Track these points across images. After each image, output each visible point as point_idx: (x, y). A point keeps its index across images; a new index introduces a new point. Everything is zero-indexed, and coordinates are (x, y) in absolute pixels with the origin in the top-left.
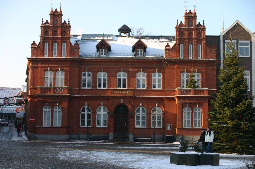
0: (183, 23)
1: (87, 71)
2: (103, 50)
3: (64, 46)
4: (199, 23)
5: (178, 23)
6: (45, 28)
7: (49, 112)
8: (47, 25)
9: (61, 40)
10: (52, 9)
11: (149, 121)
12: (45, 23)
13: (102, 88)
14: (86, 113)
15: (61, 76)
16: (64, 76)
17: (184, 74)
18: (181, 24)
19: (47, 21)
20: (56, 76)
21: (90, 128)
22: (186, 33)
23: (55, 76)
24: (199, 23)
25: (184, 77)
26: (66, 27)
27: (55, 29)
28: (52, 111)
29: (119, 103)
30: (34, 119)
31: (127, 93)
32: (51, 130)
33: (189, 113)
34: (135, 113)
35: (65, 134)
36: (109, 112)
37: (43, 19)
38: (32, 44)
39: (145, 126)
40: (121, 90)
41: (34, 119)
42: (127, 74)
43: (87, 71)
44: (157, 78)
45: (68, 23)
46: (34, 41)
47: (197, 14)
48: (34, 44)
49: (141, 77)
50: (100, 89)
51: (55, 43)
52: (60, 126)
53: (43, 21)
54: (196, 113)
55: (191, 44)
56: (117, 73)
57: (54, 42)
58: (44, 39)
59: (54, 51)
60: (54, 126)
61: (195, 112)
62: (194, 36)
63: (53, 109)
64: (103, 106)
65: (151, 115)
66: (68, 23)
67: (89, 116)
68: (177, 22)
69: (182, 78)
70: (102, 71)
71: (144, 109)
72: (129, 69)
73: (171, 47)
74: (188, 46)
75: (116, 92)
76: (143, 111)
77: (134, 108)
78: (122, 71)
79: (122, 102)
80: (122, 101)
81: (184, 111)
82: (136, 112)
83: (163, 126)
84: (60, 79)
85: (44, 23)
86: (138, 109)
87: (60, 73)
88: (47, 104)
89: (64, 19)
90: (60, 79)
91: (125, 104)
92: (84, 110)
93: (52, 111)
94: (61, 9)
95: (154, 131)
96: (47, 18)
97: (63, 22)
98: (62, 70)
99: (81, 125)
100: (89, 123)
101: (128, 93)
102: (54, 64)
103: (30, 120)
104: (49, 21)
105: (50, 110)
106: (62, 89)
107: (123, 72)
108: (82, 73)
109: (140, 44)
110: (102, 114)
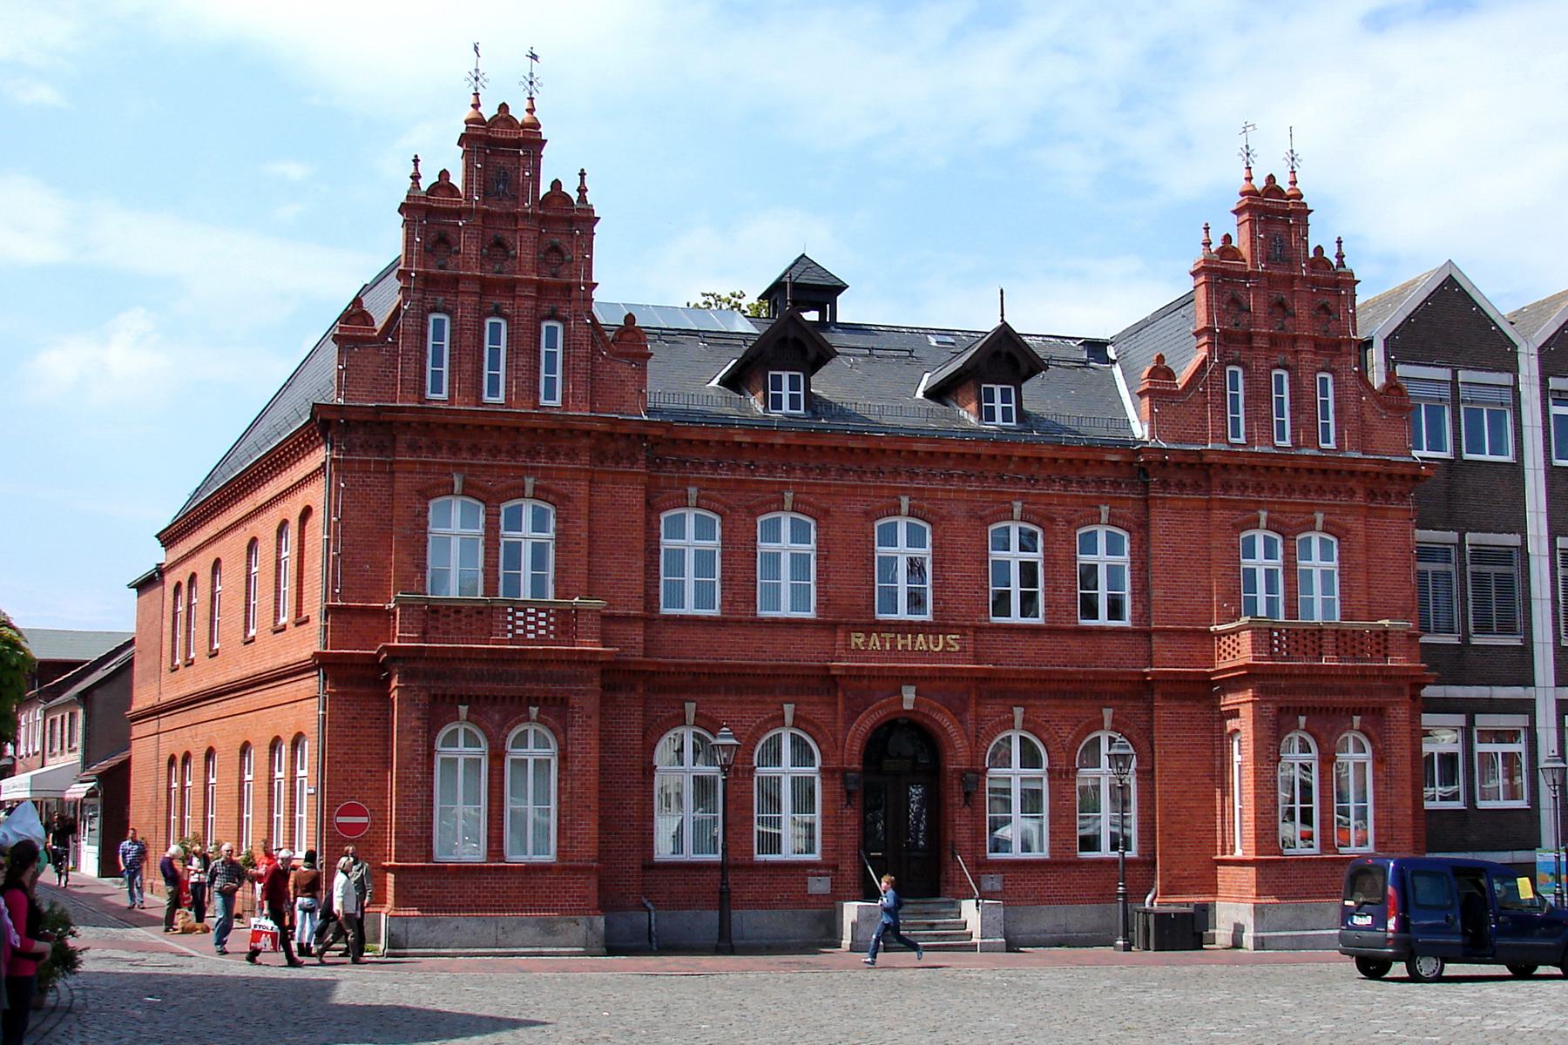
0: (1240, 241)
2: (785, 377)
3: (554, 339)
4: (556, 184)
5: (1207, 244)
6: (426, 211)
7: (473, 764)
8: (441, 201)
9: (537, 299)
10: (476, 106)
12: (433, 189)
13: (1015, 618)
15: (531, 530)
18: (1227, 250)
19: (444, 174)
22: (468, 246)
24: (556, 184)
26: (570, 221)
27: (496, 222)
28: (497, 756)
29: (897, 708)
30: (364, 820)
33: (473, 764)
36: (833, 764)
37: (416, 161)
38: (346, 317)
39: (716, 852)
40: (1102, 631)
41: (364, 820)
45: (575, 196)
46: (1160, 358)
47: (545, 132)
48: (355, 314)
49: (690, 540)
50: (999, 627)
52: (550, 857)
53: (416, 177)
55: (445, 311)
57: (547, 312)
58: (1228, 340)
60: (514, 857)
62: (1303, 319)
64: (794, 726)
66: (575, 196)
68: (412, 170)
71: (1033, 746)
73: (1182, 379)
74: (424, 325)
76: (1030, 759)
77: (977, 742)
79: (908, 706)
80: (909, 694)
81: (442, 752)
83: (823, 852)
84: (455, 544)
85: (424, 185)
89: (557, 167)
90: (455, 544)
91: (925, 715)
93: (497, 756)
94: (531, 111)
95: (724, 877)
97: (545, 188)
98: (540, 493)
101: (946, 644)
102: (496, 452)
103: (364, 814)
104: (457, 180)
105: (481, 751)
106: (543, 615)
108: (663, 517)
109: (1004, 350)
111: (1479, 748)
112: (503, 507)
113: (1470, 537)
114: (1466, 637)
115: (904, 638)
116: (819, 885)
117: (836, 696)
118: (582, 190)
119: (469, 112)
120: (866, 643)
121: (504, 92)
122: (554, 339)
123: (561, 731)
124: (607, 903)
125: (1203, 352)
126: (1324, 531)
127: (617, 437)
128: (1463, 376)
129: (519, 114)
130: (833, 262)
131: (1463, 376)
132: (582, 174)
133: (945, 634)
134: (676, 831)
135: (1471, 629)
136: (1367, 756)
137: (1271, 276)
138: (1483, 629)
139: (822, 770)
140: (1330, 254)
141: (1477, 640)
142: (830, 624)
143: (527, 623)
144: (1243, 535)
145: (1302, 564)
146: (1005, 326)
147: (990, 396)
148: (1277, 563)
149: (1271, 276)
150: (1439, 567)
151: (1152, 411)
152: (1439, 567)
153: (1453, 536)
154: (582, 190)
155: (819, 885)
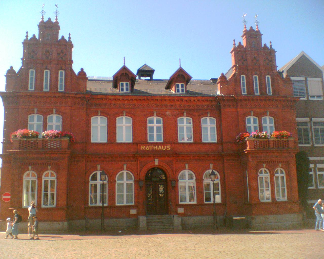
1: (99, 114)
2: (125, 83)
4: (63, 37)
5: (235, 44)
11: (200, 192)
14: (98, 182)
16: (130, 125)
17: (34, 116)
20: (48, 123)
21: (106, 207)
23: (46, 122)
24: (63, 37)
25: (249, 122)
26: (67, 46)
31: (164, 148)
32: (274, 207)
34: (115, 181)
35: (62, 221)
42: (62, 118)
43: (99, 114)
44: (155, 125)
51: (47, 70)
53: (27, 36)
54: (277, 178)
56: (148, 119)
59: (243, 86)
61: (276, 175)
63: (42, 176)
64: (127, 170)
65: (203, 182)
67: (103, 186)
69: (248, 125)
70: (124, 114)
72: (166, 112)
75: (160, 146)
78: (155, 114)
82: (116, 179)
86: (120, 174)
87: (55, 116)
88: (30, 168)
89: (63, 33)
92: (94, 178)
94: (57, 19)
96: (34, 32)
97: (60, 37)
98: (57, 113)
99: (206, 201)
100: (103, 199)
101: (167, 148)
103: (4, 198)
104: (37, 37)
107: (157, 116)
110: (125, 181)
111: (318, 173)
112: (48, 117)
113: (313, 119)
114: (313, 144)
115: (156, 147)
116: (133, 212)
117: (137, 162)
118: (70, 38)
119: (41, 20)
120: (145, 148)
121: (50, 15)
122: (61, 74)
123: (57, 172)
124: (69, 218)
125: (234, 72)
126: (269, 116)
127: (80, 98)
128: (309, 79)
129: (54, 20)
130: (152, 66)
131: (309, 79)
132: (70, 34)
133: (166, 145)
134: (96, 200)
135: (314, 143)
136: (284, 175)
137: (253, 55)
138: (317, 143)
139: (134, 181)
140: (268, 45)
141: (316, 145)
142: (136, 143)
143: (54, 144)
144: (247, 118)
145: (264, 125)
146: (180, 67)
147: (178, 86)
148: (257, 125)
149: (253, 55)
150: (305, 127)
151: (220, 87)
152: (305, 127)
153: (308, 119)
154: (70, 38)
155: (133, 212)
